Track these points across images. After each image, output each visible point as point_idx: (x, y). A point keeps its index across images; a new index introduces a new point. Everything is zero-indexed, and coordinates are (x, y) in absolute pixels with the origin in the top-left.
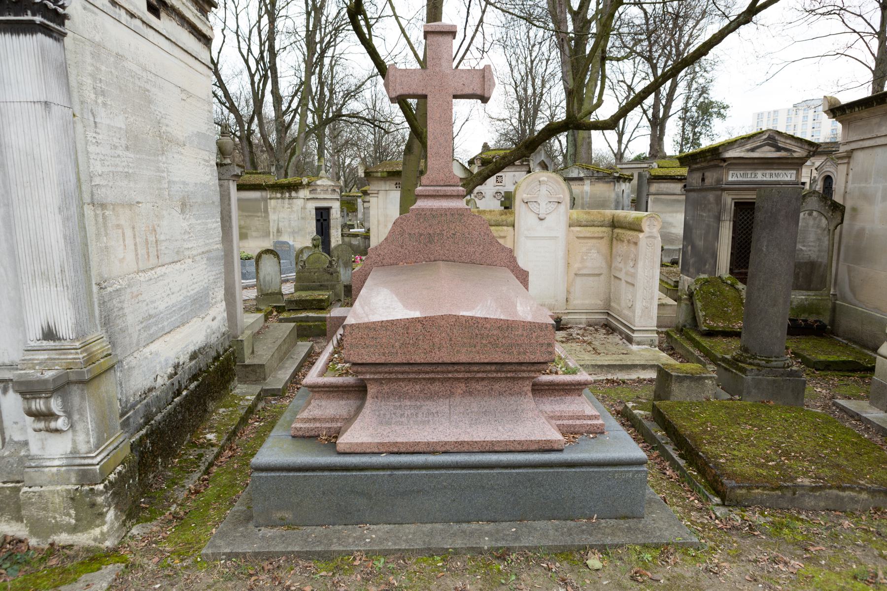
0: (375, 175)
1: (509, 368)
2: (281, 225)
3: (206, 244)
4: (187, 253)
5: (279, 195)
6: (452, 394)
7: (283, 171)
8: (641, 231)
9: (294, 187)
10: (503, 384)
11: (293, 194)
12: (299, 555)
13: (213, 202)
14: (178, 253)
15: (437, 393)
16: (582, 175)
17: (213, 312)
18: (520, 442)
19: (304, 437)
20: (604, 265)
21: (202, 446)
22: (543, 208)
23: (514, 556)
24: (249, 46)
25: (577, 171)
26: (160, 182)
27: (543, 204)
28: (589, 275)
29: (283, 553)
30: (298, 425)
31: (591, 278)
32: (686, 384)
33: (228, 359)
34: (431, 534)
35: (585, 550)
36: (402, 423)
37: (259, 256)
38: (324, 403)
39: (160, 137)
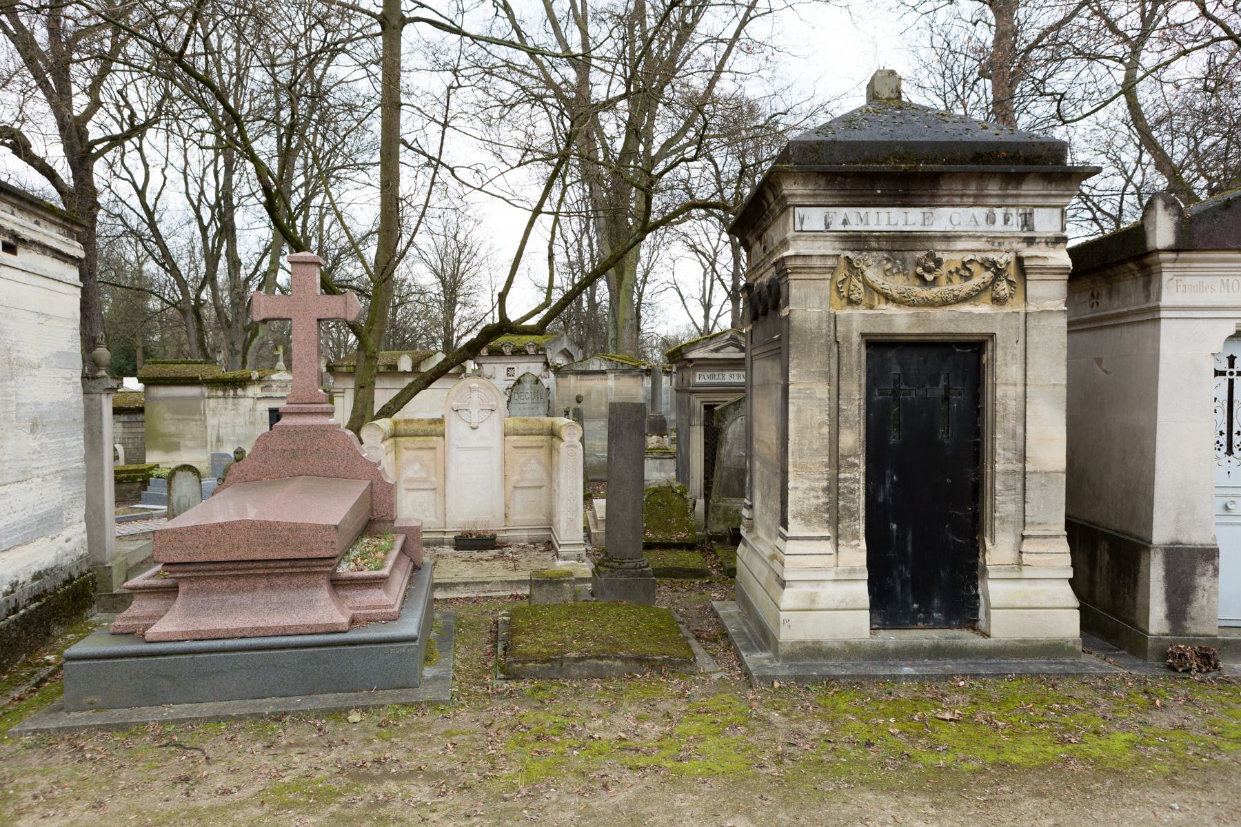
0: (340, 369)
1: (301, 563)
2: (222, 431)
3: (62, 463)
4: (35, 472)
5: (220, 393)
6: (256, 588)
7: (239, 359)
8: (561, 439)
9: (241, 383)
10: (301, 578)
11: (240, 392)
12: (99, 728)
13: (75, 420)
14: (24, 472)
15: (241, 588)
16: (604, 368)
17: (66, 533)
18: (308, 626)
19: (122, 634)
20: (544, 476)
21: (38, 665)
22: (475, 416)
23: (288, 718)
24: (202, 188)
25: (598, 363)
26: (6, 406)
27: (475, 412)
28: (529, 488)
29: (84, 727)
30: (117, 623)
31: (532, 491)
32: (545, 587)
33: (84, 584)
34: (225, 707)
35: (348, 710)
36: (208, 615)
37: (173, 473)
38: (144, 604)
39: (10, 363)
